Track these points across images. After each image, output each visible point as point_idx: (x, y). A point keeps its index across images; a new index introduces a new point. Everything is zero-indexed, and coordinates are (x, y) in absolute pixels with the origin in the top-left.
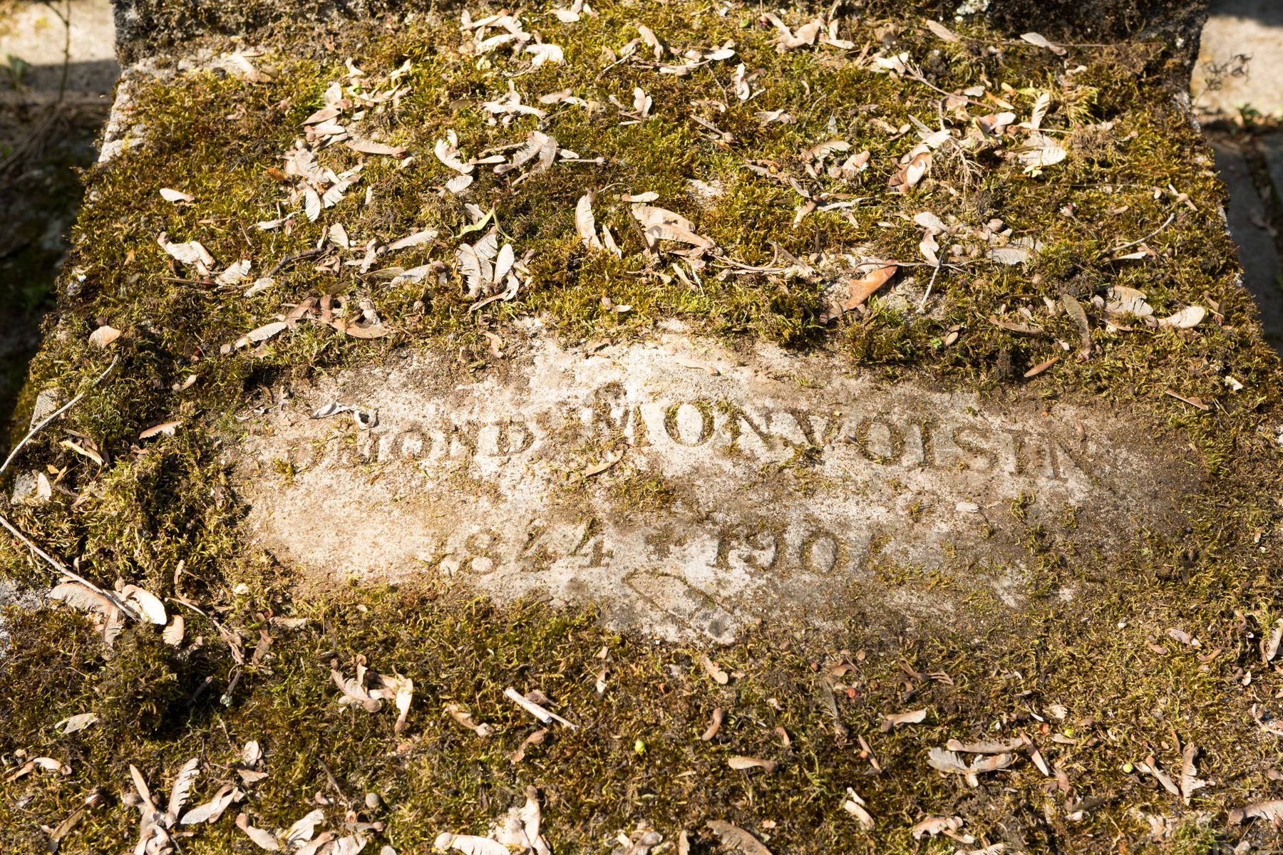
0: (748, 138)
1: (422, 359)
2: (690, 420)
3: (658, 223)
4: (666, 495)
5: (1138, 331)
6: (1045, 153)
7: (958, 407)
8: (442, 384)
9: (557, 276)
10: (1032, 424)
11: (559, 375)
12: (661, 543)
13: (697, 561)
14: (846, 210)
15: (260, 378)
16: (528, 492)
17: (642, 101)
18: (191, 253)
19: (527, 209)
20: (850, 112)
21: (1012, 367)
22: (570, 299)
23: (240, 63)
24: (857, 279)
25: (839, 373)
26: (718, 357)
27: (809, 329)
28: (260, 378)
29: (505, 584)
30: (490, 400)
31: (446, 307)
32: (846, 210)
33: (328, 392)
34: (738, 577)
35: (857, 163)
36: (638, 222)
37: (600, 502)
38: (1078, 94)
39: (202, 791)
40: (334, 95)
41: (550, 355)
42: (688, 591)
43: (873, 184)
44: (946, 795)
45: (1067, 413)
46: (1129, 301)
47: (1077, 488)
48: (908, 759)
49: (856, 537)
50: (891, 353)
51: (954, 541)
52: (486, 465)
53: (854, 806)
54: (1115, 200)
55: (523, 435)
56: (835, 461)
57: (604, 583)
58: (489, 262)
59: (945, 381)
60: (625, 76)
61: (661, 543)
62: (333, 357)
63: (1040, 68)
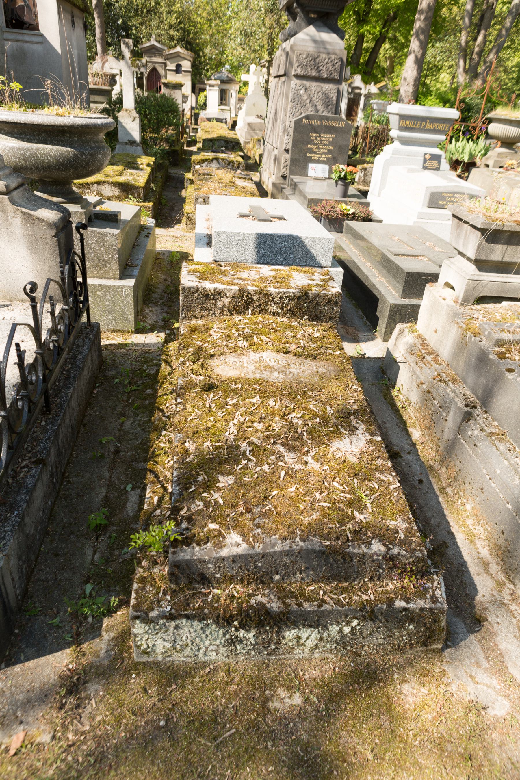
0: (276, 331)
1: (234, 354)
2: (272, 360)
3: (264, 339)
4: (270, 367)
5: (330, 354)
6: (317, 335)
7: (308, 361)
8: (238, 356)
9: (252, 345)
10: (318, 364)
11: (254, 356)
12: (271, 372)
13: (276, 374)
14: (291, 340)
15: (212, 356)
16: (252, 367)
17: (261, 326)
18: (198, 343)
19: (247, 338)
20: (29, 746)
21: (315, 358)
22: (255, 347)
23: (200, 322)
24: (292, 347)
25: (291, 356)
26: (276, 354)
27: (287, 352)
28: (212, 356)
29: (251, 376)
30: (244, 358)
31: (237, 347)
32: (291, 340)
33: (222, 358)
34: (281, 376)
35: (291, 334)
36: (20, 558)
37: (262, 368)
38: (321, 328)
39: (214, 396)
40: (215, 326)
41: (252, 353)
42: (275, 377)
43: (294, 337)
44: (310, 397)
45: (322, 363)
46: (329, 351)
47: (324, 370)
48: (305, 393)
49: (296, 373)
50: (297, 355)
51: (309, 375)
52: (245, 365)
53: (299, 397)
54: (327, 341)
55: (104, 522)
56: (292, 366)
57: (264, 376)
58: (242, 343)
59: (306, 358)
60: (258, 323)
61: (271, 372)
62: (222, 354)
63: (315, 326)
